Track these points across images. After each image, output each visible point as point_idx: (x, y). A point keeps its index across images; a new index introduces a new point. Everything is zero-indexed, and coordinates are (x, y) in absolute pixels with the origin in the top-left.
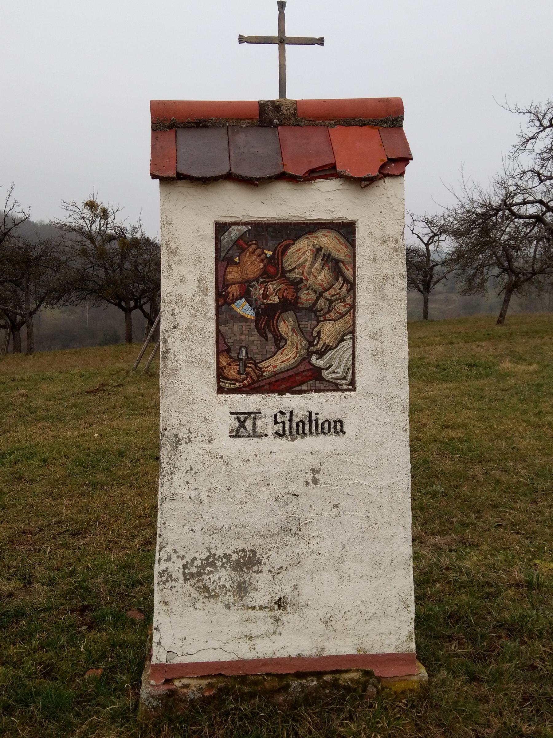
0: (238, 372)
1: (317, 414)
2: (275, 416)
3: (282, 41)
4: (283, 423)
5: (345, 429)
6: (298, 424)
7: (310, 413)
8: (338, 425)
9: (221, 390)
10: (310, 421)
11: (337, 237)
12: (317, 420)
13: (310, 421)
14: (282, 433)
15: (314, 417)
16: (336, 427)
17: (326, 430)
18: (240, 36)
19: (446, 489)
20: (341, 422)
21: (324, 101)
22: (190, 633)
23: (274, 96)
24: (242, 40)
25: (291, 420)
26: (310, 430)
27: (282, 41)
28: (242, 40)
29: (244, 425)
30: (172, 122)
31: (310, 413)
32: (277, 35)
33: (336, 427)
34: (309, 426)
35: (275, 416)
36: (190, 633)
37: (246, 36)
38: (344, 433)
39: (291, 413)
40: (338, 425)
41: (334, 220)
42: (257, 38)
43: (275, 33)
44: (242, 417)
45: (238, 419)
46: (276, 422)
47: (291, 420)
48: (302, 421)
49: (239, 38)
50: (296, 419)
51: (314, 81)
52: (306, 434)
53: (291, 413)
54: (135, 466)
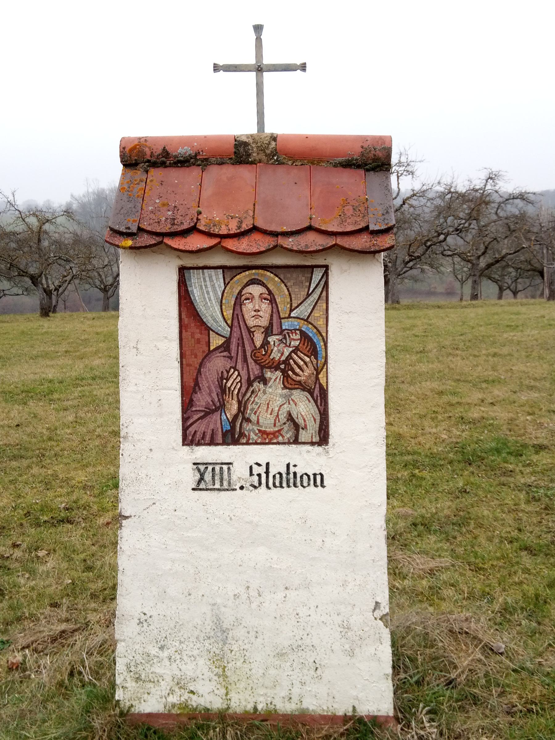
1: (295, 466)
2: (251, 468)
3: (259, 69)
4: (259, 475)
5: (325, 483)
6: (274, 477)
7: (288, 466)
9: (189, 439)
10: (288, 473)
12: (295, 474)
13: (288, 473)
14: (257, 485)
15: (292, 469)
16: (318, 480)
17: (305, 484)
18: (214, 64)
19: (283, 723)
23: (253, 130)
24: (216, 68)
25: (267, 473)
26: (281, 483)
29: (209, 479)
30: (139, 158)
32: (255, 73)
33: (318, 480)
34: (290, 479)
35: (251, 468)
39: (268, 464)
42: (263, 113)
44: (202, 468)
45: (199, 470)
46: (251, 474)
47: (267, 473)
50: (273, 471)
52: (283, 487)
53: (268, 464)
54: (88, 516)
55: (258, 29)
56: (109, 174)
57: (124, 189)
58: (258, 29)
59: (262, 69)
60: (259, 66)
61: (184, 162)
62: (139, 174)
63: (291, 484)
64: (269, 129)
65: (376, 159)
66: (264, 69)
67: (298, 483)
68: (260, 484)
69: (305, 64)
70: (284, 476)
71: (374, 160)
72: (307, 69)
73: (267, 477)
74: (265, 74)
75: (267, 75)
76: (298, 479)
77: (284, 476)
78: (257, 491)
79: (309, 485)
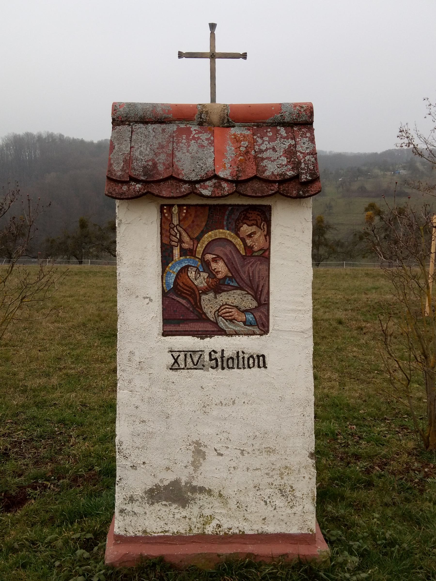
0: (182, 311)
3: (213, 56)
7: (238, 353)
8: (261, 358)
10: (238, 357)
11: (233, 252)
12: (243, 358)
15: (240, 354)
16: (260, 361)
18: (179, 52)
20: (263, 356)
21: (250, 106)
22: (137, 519)
23: (207, 101)
24: (181, 55)
25: (222, 357)
27: (213, 56)
28: (181, 55)
29: (180, 362)
31: (238, 353)
33: (260, 361)
36: (137, 519)
37: (184, 52)
38: (266, 368)
40: (261, 358)
41: (315, 505)
43: (207, 49)
47: (222, 357)
48: (232, 358)
49: (179, 54)
50: (226, 355)
51: (239, 88)
53: (223, 351)
55: (213, 26)
56: (100, 130)
57: (117, 138)
58: (213, 26)
59: (214, 56)
60: (213, 54)
61: (161, 121)
62: (126, 128)
63: (246, 366)
64: (221, 100)
65: (304, 118)
66: (217, 56)
67: (225, 365)
68: (217, 366)
69: (246, 53)
70: (219, 360)
71: (301, 121)
72: (247, 57)
73: (238, 360)
74: (217, 60)
75: (218, 61)
76: (220, 363)
77: (236, 361)
78: (259, 369)
79: (254, 366)
